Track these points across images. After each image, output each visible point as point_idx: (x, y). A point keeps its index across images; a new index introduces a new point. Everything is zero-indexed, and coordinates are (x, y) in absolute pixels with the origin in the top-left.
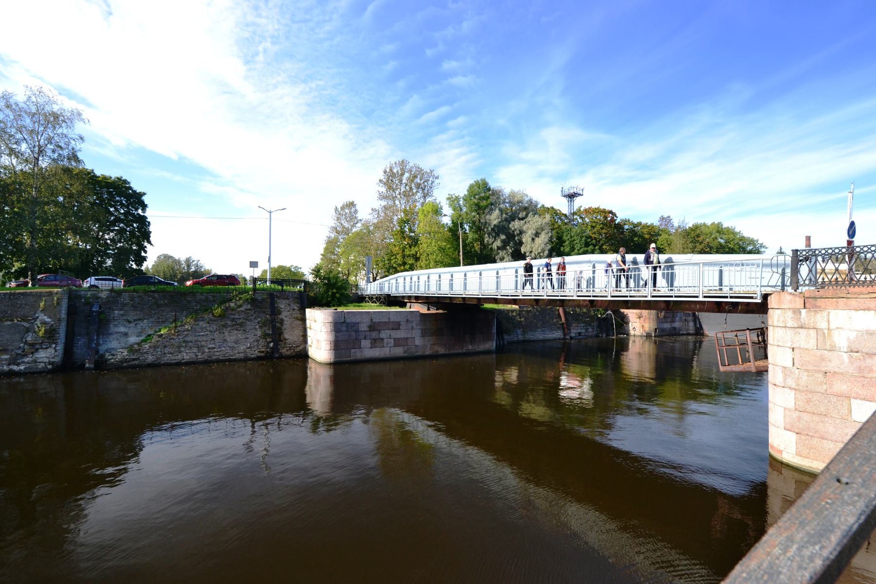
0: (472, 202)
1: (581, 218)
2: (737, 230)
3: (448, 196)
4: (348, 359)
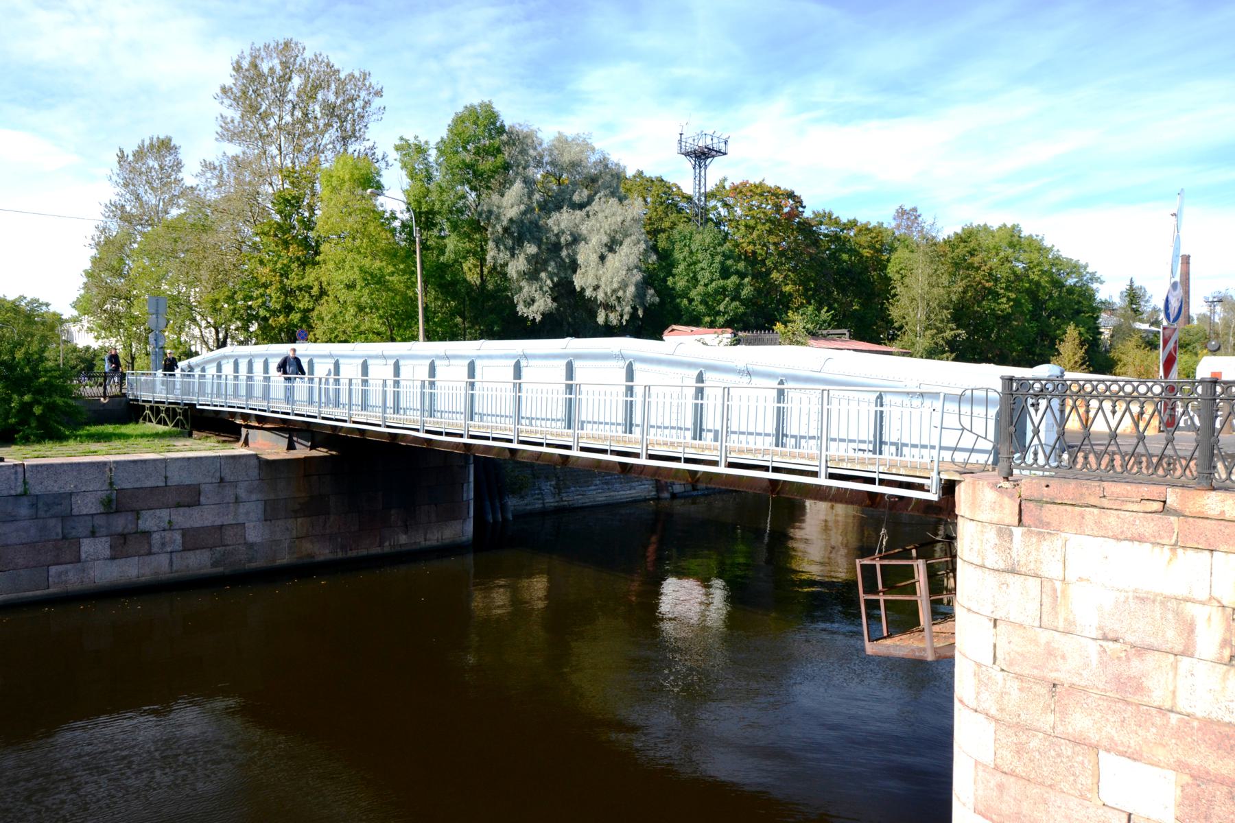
0: (456, 160)
1: (726, 205)
2: (1047, 243)
3: (398, 142)
4: (38, 593)
